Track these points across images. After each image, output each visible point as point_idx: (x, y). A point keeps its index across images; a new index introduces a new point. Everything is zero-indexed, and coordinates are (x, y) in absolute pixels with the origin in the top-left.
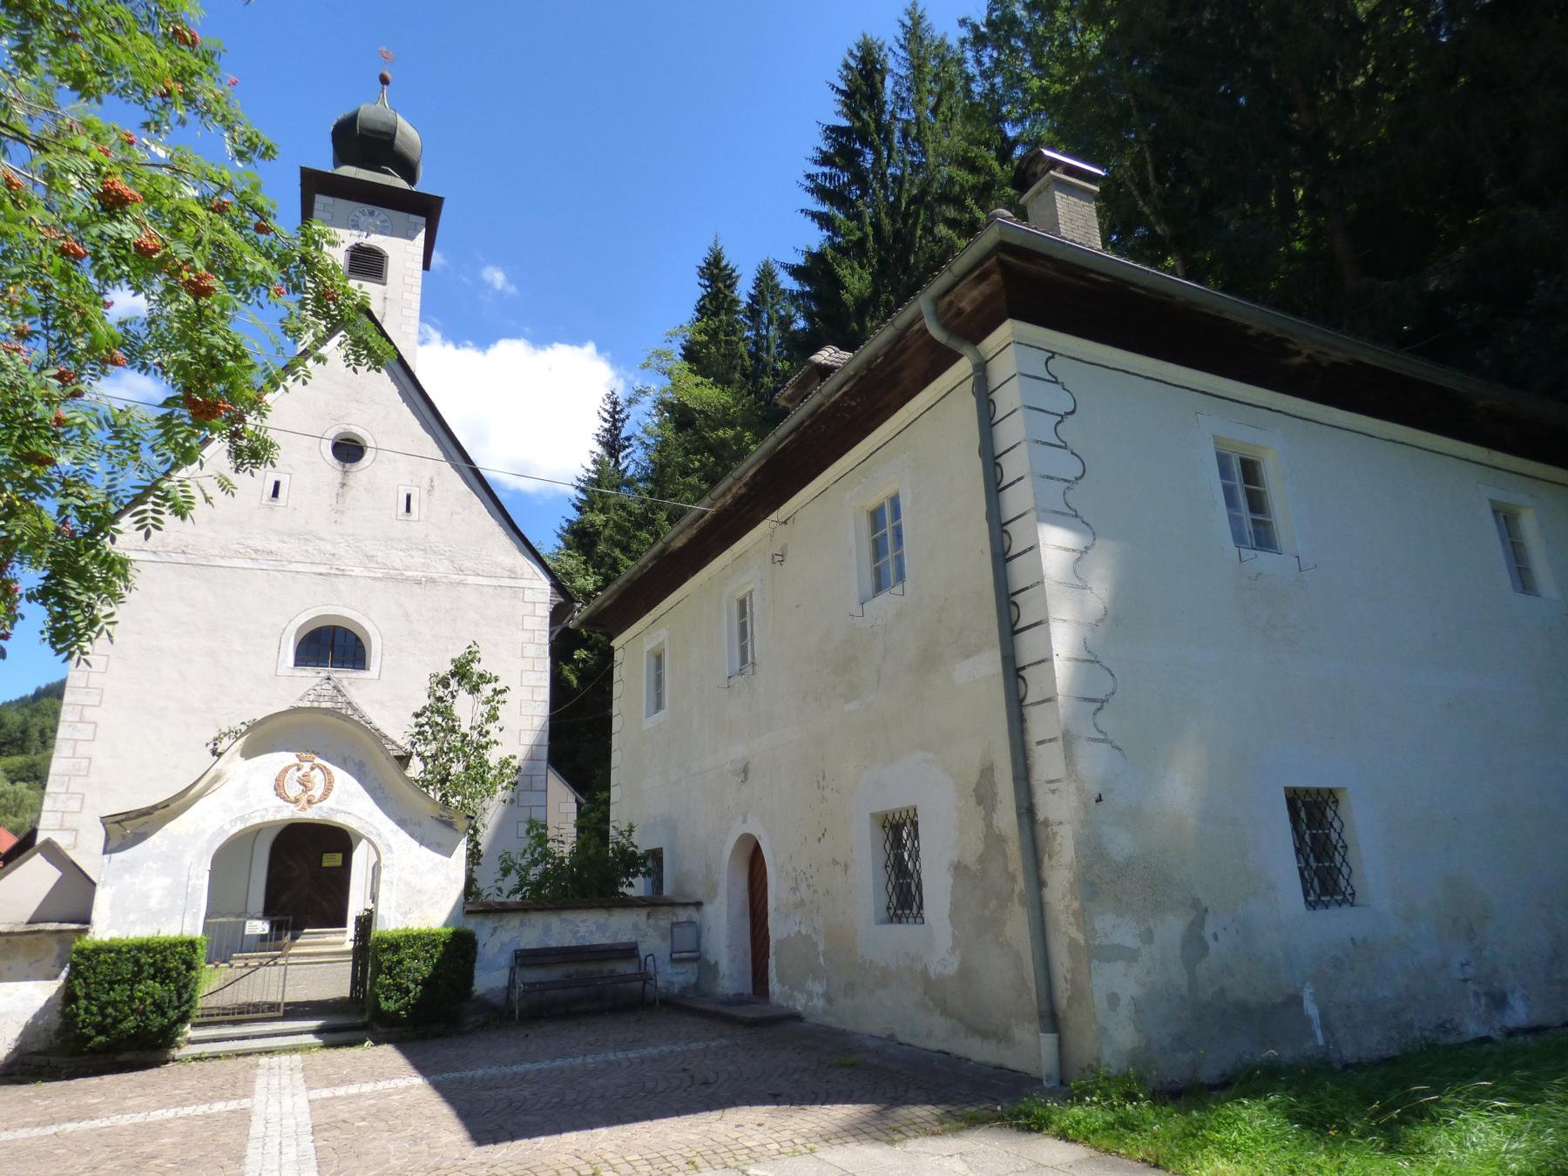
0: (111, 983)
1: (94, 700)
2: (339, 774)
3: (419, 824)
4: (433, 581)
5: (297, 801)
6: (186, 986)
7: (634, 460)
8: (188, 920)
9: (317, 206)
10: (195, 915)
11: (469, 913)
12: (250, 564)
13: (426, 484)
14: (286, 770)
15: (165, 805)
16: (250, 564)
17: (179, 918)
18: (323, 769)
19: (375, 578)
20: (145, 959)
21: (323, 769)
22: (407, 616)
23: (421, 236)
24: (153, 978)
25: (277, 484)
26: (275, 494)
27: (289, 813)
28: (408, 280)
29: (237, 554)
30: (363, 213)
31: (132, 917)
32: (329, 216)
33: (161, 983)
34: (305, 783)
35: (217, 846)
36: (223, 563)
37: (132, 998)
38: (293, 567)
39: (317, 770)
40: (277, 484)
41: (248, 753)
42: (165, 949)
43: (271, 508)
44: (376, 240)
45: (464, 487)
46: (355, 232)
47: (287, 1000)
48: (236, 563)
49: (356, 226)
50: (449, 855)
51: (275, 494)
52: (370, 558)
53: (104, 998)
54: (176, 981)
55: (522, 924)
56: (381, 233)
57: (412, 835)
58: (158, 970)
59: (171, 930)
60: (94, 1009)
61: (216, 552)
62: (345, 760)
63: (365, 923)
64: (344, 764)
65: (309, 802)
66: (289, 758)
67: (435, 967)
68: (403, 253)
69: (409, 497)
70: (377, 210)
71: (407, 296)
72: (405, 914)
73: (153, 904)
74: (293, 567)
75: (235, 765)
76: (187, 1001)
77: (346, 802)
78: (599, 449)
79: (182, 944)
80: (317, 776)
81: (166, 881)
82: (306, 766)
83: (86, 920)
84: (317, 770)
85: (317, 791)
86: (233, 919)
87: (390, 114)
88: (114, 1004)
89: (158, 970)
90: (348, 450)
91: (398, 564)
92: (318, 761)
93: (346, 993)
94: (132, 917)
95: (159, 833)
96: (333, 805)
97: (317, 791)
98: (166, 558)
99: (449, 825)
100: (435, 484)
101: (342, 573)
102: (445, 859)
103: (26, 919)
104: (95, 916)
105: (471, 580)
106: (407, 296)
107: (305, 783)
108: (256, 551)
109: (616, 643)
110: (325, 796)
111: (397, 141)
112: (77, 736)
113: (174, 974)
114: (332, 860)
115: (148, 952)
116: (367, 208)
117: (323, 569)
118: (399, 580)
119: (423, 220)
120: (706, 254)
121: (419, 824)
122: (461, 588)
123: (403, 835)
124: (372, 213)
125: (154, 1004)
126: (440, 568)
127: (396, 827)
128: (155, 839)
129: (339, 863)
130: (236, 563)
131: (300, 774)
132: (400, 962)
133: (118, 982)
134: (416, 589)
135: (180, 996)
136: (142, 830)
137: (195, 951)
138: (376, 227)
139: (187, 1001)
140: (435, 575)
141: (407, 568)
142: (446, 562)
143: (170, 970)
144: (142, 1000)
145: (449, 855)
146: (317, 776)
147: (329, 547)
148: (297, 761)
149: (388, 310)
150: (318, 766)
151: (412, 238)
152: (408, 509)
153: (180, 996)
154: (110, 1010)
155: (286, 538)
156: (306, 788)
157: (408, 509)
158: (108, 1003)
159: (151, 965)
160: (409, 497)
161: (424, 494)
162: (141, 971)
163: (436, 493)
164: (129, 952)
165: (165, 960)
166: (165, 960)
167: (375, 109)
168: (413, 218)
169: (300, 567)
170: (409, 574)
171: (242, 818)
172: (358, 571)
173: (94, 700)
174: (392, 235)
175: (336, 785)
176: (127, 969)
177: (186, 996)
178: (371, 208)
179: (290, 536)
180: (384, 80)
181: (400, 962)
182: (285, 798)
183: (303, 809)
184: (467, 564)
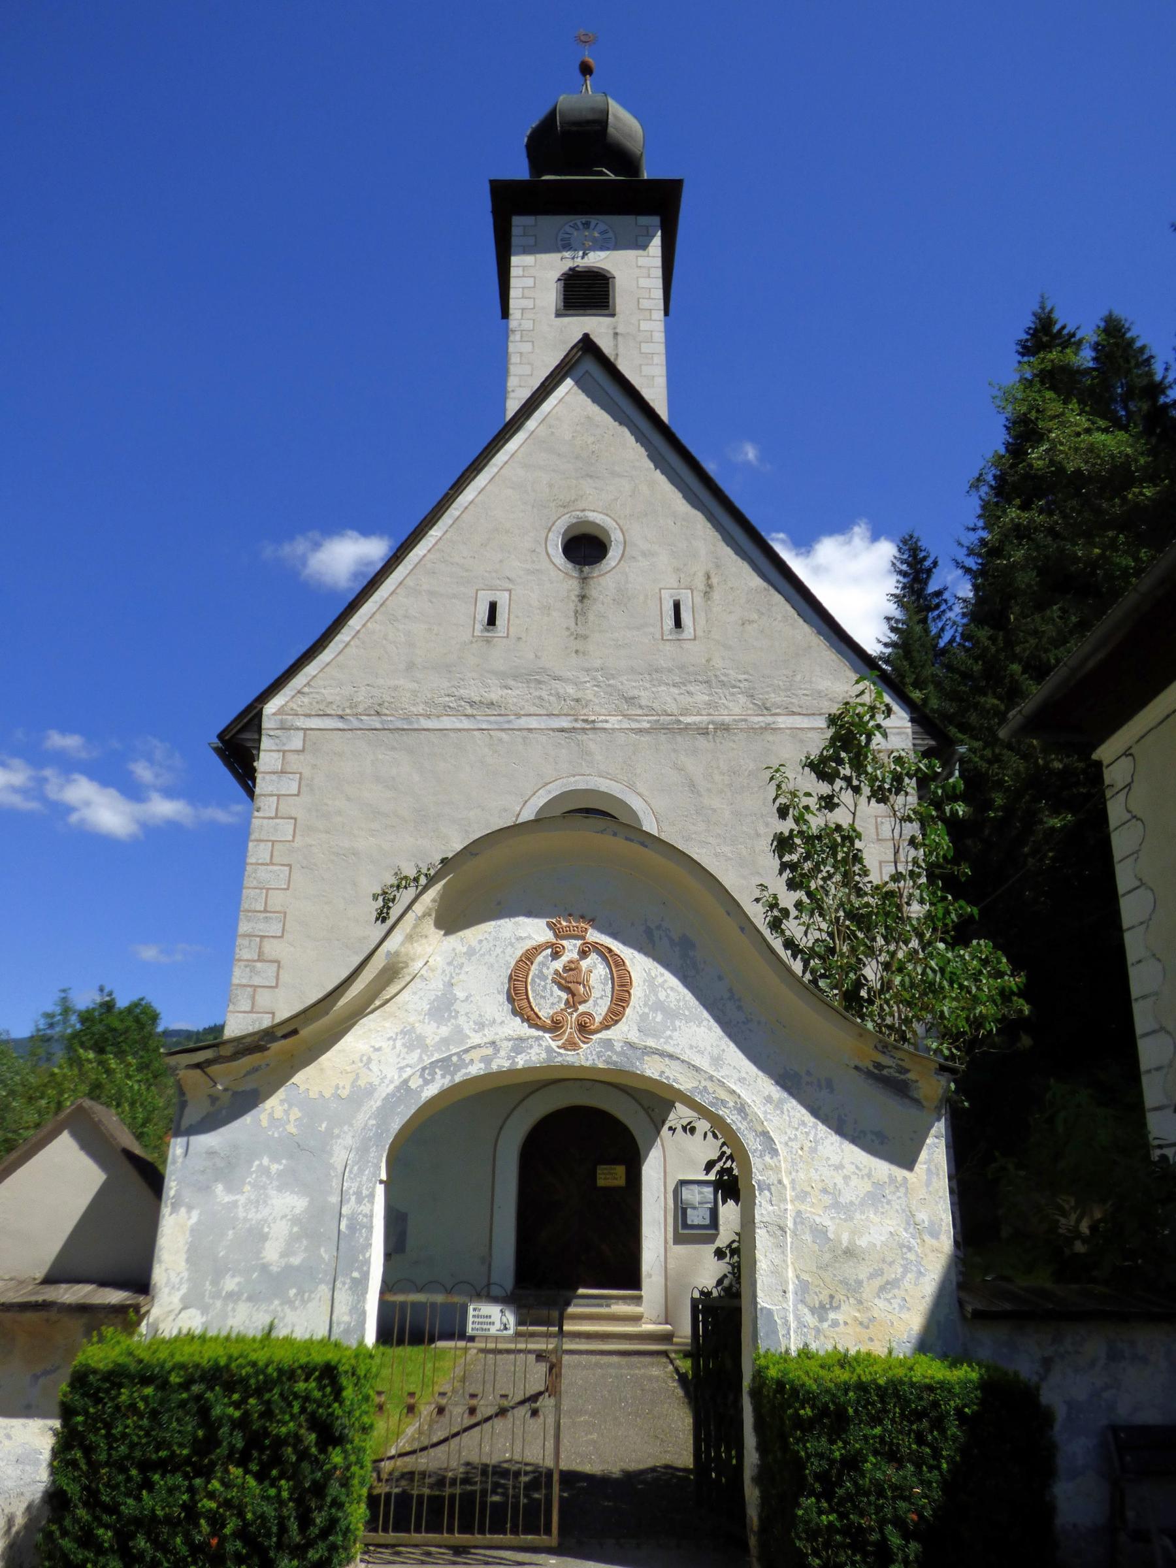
0: (146, 1466)
1: (275, 928)
2: (639, 964)
3: (830, 1085)
4: (725, 728)
5: (555, 1027)
6: (319, 1489)
7: (951, 622)
8: (343, 1298)
9: (515, 231)
10: (360, 1286)
11: (978, 1315)
12: (466, 724)
13: (700, 583)
14: (528, 957)
15: (288, 1029)
16: (466, 724)
17: (324, 1290)
18: (606, 955)
19: (640, 731)
20: (223, 1408)
21: (606, 955)
22: (692, 786)
23: (657, 242)
24: (243, 1461)
25: (493, 607)
26: (492, 621)
27: (539, 1051)
28: (645, 304)
29: (448, 711)
30: (575, 227)
31: (230, 1284)
32: (531, 241)
33: (260, 1477)
34: (570, 984)
35: (396, 1125)
36: (425, 723)
37: (191, 1512)
38: (524, 722)
39: (593, 958)
40: (493, 607)
41: (452, 919)
42: (267, 1385)
43: (488, 641)
44: (597, 259)
45: (757, 582)
46: (567, 254)
47: (564, 1466)
48: (447, 722)
49: (567, 246)
50: (909, 1165)
51: (492, 621)
52: (630, 700)
53: (129, 1506)
54: (294, 1475)
55: (1114, 1356)
56: (602, 249)
57: (815, 1112)
58: (255, 1440)
59: (305, 1322)
60: (105, 1535)
61: (420, 709)
62: (649, 932)
63: (722, 1318)
64: (647, 945)
65: (583, 1029)
66: (534, 930)
67: (947, 1486)
68: (635, 270)
69: (677, 607)
70: (593, 220)
71: (645, 326)
72: (821, 1311)
73: (272, 1253)
74: (524, 722)
75: (430, 951)
76: (325, 1533)
77: (665, 1029)
78: (1002, 451)
79: (308, 1371)
80: (596, 971)
81: (297, 1203)
82: (571, 949)
83: (142, 1285)
84: (593, 958)
85: (598, 1006)
86: (439, 1298)
87: (599, 97)
88: (148, 1524)
89: (255, 1440)
90: (585, 548)
91: (672, 707)
92: (594, 936)
93: (684, 1458)
94: (230, 1284)
95: (281, 1093)
96: (634, 1037)
97: (598, 1006)
98: (355, 723)
99: (899, 1087)
100: (714, 580)
101: (592, 727)
102: (900, 1173)
103: (40, 1274)
104: (159, 1275)
105: (783, 722)
106: (644, 282)
107: (570, 984)
108: (472, 704)
109: (1104, 753)
110: (615, 1016)
111: (611, 130)
112: (257, 981)
113: (289, 1452)
114: (611, 1176)
115: (229, 1388)
116: (579, 220)
117: (565, 723)
118: (670, 729)
119: (656, 220)
120: (1029, 322)
121: (830, 1085)
122: (770, 737)
123: (797, 1111)
124: (587, 225)
125: (241, 1533)
126: (734, 708)
127: (776, 1092)
128: (274, 1105)
129: (621, 1181)
130: (447, 722)
131: (558, 965)
132: (852, 1463)
133: (163, 1466)
134: (702, 742)
135: (305, 1521)
136: (248, 1085)
137: (338, 1392)
138: (595, 240)
139: (325, 1533)
140: (727, 719)
141: (685, 712)
142: (742, 699)
143: (280, 1442)
144: (216, 1522)
145: (909, 1165)
146: (596, 971)
147: (570, 690)
148: (549, 936)
149: (621, 350)
150: (597, 948)
151: (644, 247)
152: (678, 623)
153: (305, 1521)
154: (141, 1543)
155: (511, 683)
156: (575, 999)
157: (678, 623)
158: (138, 1522)
159: (236, 1424)
160: (677, 607)
161: (699, 599)
162: (210, 1442)
163: (716, 596)
164: (186, 1386)
165: (268, 1414)
166: (268, 1414)
167: (579, 98)
168: (644, 220)
169: (533, 723)
170: (689, 720)
171: (445, 1064)
172: (614, 722)
173: (275, 928)
174: (616, 247)
175: (638, 992)
176: (181, 1432)
177: (319, 1519)
178: (584, 218)
179: (515, 677)
180: (586, 69)
181: (852, 1463)
182: (531, 1019)
183: (571, 1045)
184: (774, 698)
